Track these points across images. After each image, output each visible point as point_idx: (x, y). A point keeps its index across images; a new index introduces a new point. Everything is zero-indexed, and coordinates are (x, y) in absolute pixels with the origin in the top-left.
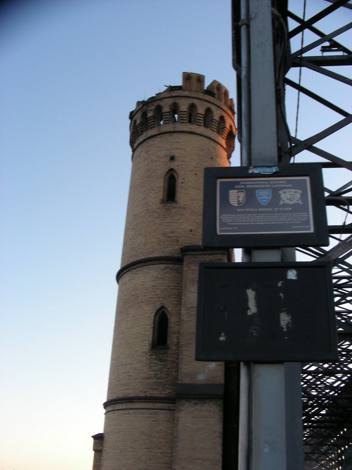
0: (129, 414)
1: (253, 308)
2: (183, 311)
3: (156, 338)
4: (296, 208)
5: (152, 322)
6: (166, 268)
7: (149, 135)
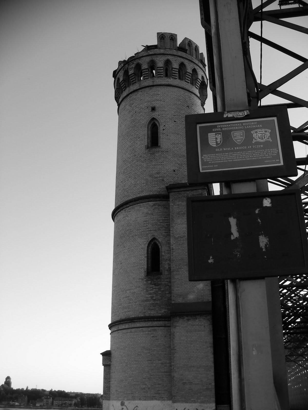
0: (131, 332)
1: (235, 234)
2: (172, 241)
4: (266, 145)
6: (154, 205)
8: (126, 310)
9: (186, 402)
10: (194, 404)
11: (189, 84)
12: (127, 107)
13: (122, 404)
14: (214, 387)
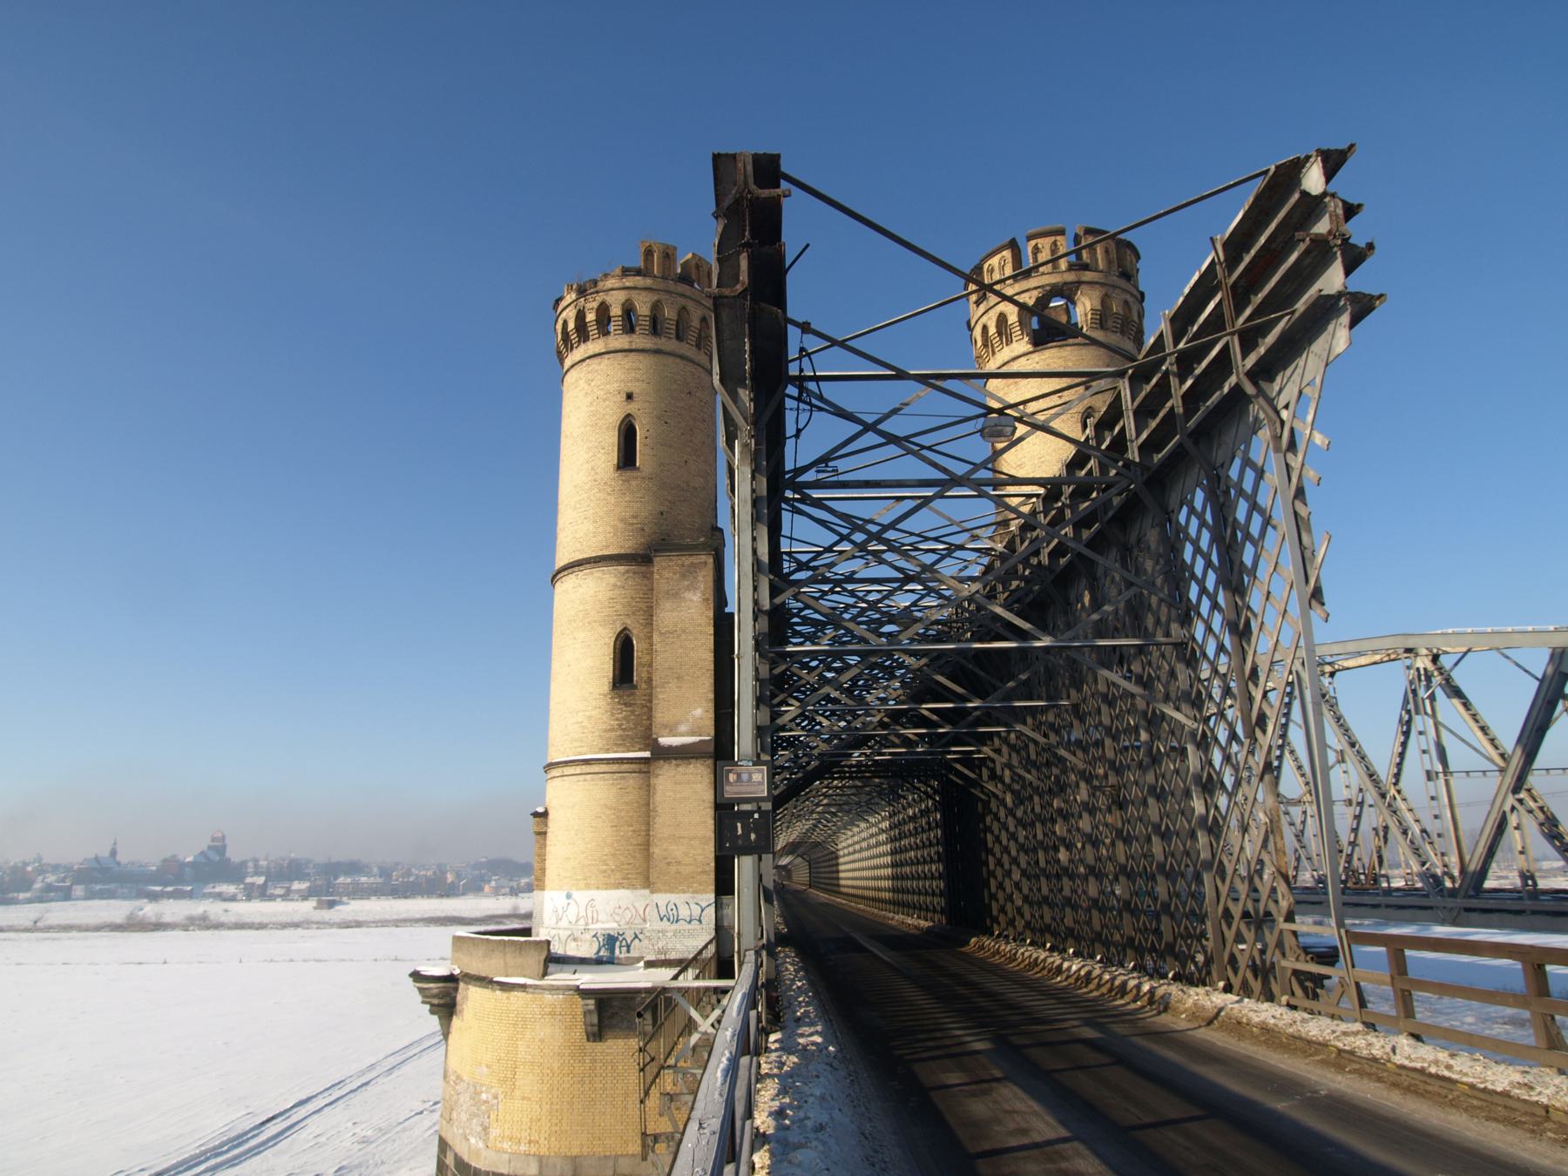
0: (585, 780)
1: (740, 832)
2: (656, 638)
3: (617, 672)
4: (760, 783)
5: (612, 650)
6: (627, 572)
7: (591, 353)
8: (576, 744)
9: (671, 891)
10: (682, 895)
11: (694, 348)
12: (582, 383)
13: (569, 896)
14: (713, 869)
